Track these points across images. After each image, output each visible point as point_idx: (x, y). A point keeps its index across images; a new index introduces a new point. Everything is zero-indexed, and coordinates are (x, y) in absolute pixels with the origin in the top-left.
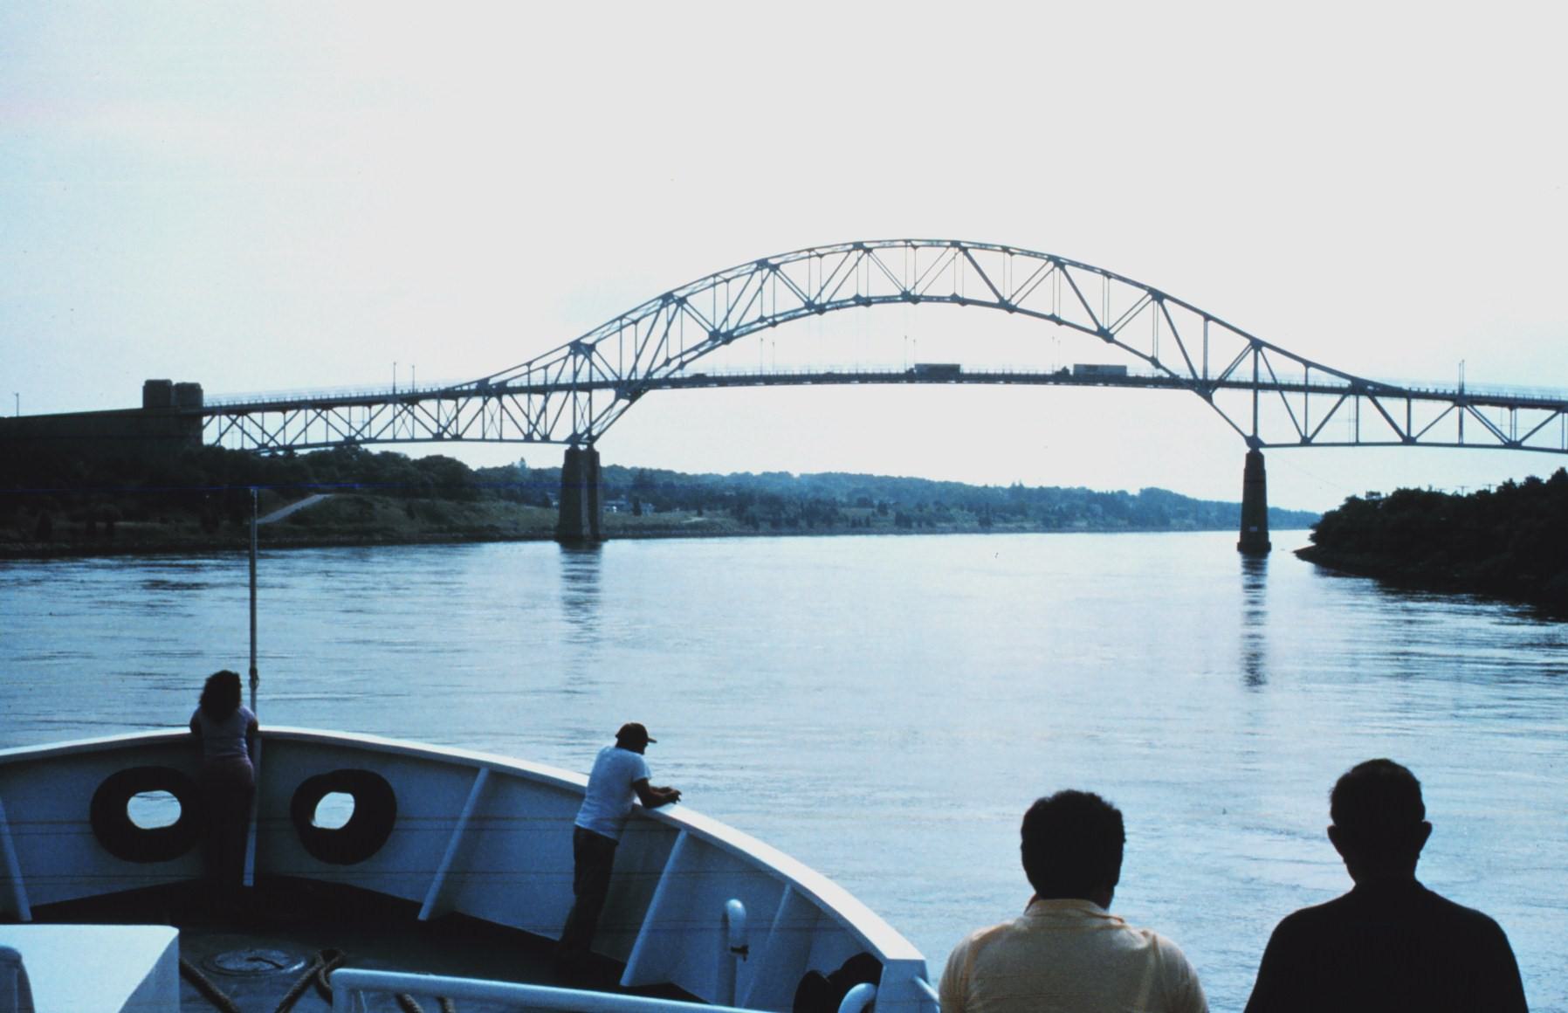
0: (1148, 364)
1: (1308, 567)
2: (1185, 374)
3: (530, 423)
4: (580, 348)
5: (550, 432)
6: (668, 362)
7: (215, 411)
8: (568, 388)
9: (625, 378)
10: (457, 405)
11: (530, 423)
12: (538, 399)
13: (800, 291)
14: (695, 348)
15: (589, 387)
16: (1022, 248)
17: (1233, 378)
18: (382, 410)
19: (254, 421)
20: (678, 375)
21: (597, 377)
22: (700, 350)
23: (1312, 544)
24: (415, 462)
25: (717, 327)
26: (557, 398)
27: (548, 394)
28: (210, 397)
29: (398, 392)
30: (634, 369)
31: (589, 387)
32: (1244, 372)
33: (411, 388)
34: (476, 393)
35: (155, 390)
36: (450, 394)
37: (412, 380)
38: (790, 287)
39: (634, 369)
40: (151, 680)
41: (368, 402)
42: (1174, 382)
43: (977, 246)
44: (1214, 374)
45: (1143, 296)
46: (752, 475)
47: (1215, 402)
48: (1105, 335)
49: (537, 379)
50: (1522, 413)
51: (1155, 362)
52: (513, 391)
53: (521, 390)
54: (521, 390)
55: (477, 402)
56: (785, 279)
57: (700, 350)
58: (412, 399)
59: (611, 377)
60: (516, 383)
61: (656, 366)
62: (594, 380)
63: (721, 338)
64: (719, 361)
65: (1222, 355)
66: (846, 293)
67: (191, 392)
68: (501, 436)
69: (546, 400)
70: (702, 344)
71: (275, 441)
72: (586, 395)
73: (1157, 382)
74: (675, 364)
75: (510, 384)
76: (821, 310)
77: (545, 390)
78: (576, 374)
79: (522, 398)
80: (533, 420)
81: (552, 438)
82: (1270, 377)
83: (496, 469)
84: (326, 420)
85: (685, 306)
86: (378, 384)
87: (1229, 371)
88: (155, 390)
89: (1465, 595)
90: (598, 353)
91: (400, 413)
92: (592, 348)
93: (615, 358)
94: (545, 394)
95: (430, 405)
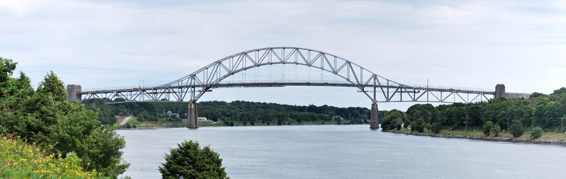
0: (346, 80)
1: (370, 129)
2: (356, 83)
4: (193, 76)
13: (314, 62)
17: (369, 84)
21: (197, 84)
23: (120, 150)
24: (274, 104)
31: (194, 87)
32: (372, 82)
38: (314, 62)
40: (176, 166)
42: (353, 85)
44: (364, 84)
45: (313, 64)
46: (316, 107)
48: (335, 73)
50: (373, 93)
56: (313, 61)
65: (366, 78)
72: (181, 89)
75: (171, 86)
76: (258, 66)
87: (368, 82)
93: (202, 79)
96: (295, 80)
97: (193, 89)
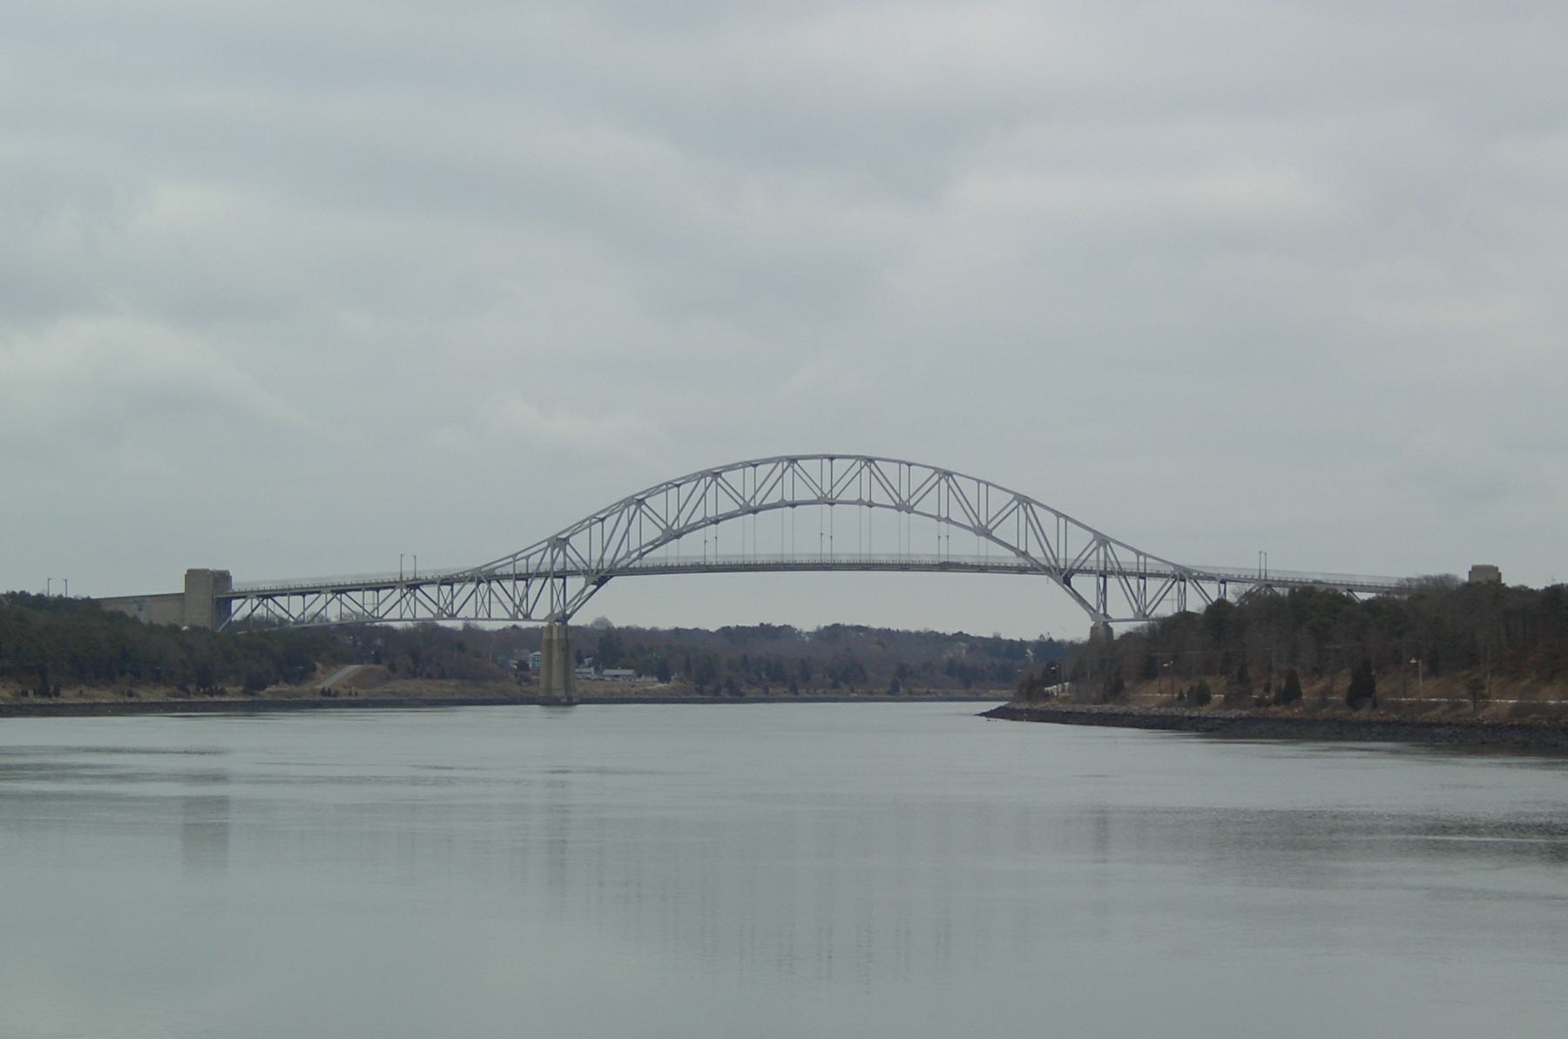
3: (515, 604)
4: (559, 542)
5: (531, 612)
6: (629, 554)
7: (244, 596)
8: (546, 575)
9: (594, 566)
10: (452, 589)
11: (515, 604)
12: (521, 584)
14: (652, 543)
15: (563, 574)
16: (683, 475)
18: (316, 599)
19: (278, 604)
20: (637, 564)
21: (569, 567)
22: (656, 544)
25: (670, 523)
26: (538, 583)
27: (530, 580)
28: (239, 581)
29: (707, 564)
30: (602, 560)
31: (563, 574)
33: (412, 576)
34: (471, 580)
35: (192, 576)
36: (448, 581)
37: (399, 570)
39: (602, 560)
41: (377, 588)
42: (1036, 568)
43: (735, 467)
45: (918, 505)
47: (1072, 585)
48: (985, 532)
49: (521, 567)
51: (1025, 554)
52: (499, 579)
53: (508, 577)
54: (508, 577)
55: (471, 587)
57: (656, 544)
58: (414, 585)
59: (582, 566)
60: (504, 571)
61: (619, 557)
62: (568, 569)
63: (672, 535)
64: (671, 552)
65: (1075, 546)
66: (774, 498)
67: (223, 578)
68: (414, 616)
69: (527, 586)
70: (657, 540)
71: (1168, 600)
73: (1021, 570)
74: (635, 555)
75: (498, 572)
77: (526, 577)
78: (553, 562)
79: (508, 585)
80: (517, 601)
81: (533, 617)
82: (503, 584)
83: (654, 633)
84: (340, 600)
85: (643, 507)
86: (386, 569)
88: (192, 576)
89: (267, 699)
90: (570, 545)
91: (405, 595)
92: (566, 540)
93: (585, 549)
94: (527, 580)
95: (431, 590)
96: (939, 555)
97: (1222, 586)
